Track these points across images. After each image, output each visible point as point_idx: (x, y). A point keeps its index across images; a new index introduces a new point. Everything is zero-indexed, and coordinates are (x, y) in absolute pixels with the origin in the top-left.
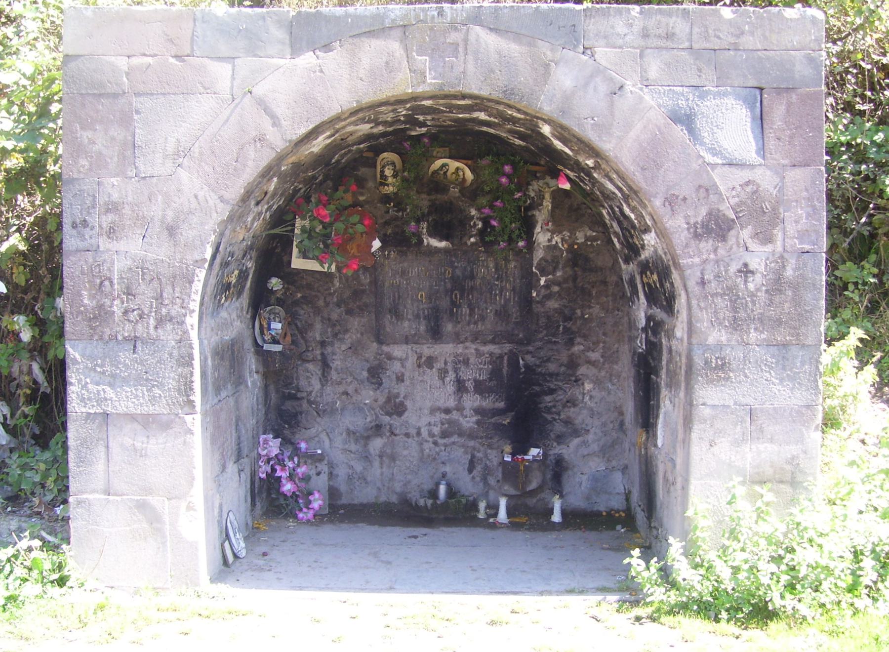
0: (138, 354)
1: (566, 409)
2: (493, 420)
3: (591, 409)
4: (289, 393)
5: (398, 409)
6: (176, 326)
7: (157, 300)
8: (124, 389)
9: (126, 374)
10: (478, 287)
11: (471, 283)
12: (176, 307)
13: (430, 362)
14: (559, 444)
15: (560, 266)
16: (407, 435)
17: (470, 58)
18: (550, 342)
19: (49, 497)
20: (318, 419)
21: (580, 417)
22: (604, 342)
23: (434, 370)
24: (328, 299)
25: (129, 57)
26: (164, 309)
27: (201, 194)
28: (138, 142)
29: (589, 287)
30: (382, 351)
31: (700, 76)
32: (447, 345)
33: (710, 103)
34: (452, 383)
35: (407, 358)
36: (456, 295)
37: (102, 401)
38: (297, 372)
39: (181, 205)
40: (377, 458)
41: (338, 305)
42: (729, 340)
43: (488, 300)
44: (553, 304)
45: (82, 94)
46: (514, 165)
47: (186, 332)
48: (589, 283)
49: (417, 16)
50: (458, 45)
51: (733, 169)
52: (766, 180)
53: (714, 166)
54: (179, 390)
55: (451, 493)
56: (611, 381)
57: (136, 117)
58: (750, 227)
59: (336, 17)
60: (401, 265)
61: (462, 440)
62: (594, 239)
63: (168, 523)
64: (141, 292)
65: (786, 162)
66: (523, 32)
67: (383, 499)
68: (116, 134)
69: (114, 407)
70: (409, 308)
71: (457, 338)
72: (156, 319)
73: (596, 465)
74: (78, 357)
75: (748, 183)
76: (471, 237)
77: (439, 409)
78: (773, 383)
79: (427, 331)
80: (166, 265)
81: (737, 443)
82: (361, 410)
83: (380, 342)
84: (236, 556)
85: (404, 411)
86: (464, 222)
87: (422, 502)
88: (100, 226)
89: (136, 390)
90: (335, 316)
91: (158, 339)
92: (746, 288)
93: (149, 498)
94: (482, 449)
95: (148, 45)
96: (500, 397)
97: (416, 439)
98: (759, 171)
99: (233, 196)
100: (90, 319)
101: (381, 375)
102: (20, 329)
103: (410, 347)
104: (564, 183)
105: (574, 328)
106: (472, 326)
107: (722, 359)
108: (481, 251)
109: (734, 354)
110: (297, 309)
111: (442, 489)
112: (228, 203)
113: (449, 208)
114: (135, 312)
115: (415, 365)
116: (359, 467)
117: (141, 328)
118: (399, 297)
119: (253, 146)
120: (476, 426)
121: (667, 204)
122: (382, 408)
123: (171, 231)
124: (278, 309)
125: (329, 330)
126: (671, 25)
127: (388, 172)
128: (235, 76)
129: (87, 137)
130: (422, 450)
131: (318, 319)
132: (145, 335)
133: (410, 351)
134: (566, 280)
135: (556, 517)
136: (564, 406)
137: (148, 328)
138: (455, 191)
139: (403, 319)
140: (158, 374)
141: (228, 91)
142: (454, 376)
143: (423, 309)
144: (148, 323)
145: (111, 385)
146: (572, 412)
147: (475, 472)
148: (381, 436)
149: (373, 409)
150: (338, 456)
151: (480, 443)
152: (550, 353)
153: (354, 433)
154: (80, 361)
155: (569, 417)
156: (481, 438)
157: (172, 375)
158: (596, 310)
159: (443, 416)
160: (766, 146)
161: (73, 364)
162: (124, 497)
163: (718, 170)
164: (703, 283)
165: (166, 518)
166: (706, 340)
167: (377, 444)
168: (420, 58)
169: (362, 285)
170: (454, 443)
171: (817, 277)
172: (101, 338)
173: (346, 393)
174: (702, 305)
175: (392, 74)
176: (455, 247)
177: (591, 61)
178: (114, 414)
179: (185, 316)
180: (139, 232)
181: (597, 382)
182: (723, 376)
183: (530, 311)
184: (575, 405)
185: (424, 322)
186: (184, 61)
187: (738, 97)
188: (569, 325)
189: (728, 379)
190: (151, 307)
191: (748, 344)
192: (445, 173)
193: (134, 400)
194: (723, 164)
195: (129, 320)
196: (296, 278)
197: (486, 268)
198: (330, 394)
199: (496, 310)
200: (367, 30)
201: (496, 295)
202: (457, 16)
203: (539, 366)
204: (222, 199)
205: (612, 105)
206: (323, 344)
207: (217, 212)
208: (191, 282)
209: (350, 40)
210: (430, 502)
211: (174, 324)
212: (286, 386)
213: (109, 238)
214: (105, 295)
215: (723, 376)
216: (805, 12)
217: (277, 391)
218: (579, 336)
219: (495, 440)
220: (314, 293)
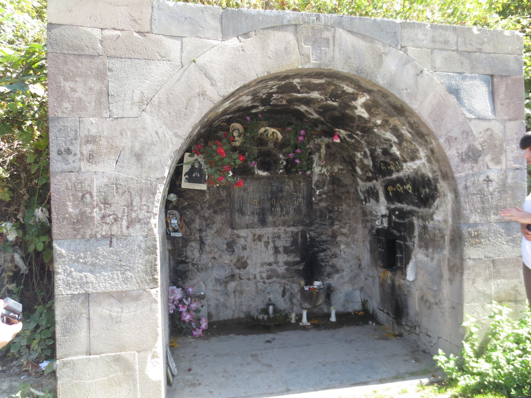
0: (114, 248)
1: (332, 260)
2: (294, 268)
3: (344, 259)
5: (242, 264)
6: (143, 226)
7: (128, 207)
8: (102, 275)
9: (104, 263)
11: (281, 195)
12: (143, 212)
13: (260, 238)
14: (329, 278)
15: (326, 184)
16: (249, 279)
17: (337, 49)
18: (322, 224)
19: (34, 356)
20: (198, 274)
21: (338, 262)
22: (349, 223)
24: (203, 206)
25: (102, 29)
26: (133, 214)
27: (160, 131)
28: (111, 92)
29: (341, 195)
31: (462, 67)
33: (468, 83)
35: (248, 237)
37: (84, 285)
39: (146, 139)
40: (232, 293)
41: (209, 209)
42: (481, 220)
44: (323, 204)
45: (64, 54)
46: (306, 130)
47: (151, 230)
48: (341, 193)
49: (303, 19)
50: (329, 40)
51: (480, 121)
52: (497, 127)
53: (470, 119)
54: (146, 271)
55: (275, 311)
56: (354, 243)
57: (109, 74)
58: (489, 155)
59: (252, 15)
61: (278, 280)
62: (342, 170)
63: (138, 370)
64: (115, 201)
65: (506, 118)
66: (367, 34)
67: (236, 316)
68: (93, 85)
69: (94, 288)
70: (248, 209)
71: (275, 224)
72: (128, 221)
73: (347, 288)
74: (64, 252)
75: (488, 130)
76: (280, 169)
77: (265, 263)
78: (503, 244)
79: (259, 221)
80: (135, 182)
81: (487, 280)
82: (223, 267)
83: (233, 228)
84: (173, 375)
85: (247, 266)
86: (277, 161)
87: (261, 317)
88: (82, 153)
89: (112, 274)
90: (207, 215)
91: (129, 235)
92: (488, 190)
93: (123, 353)
94: (289, 284)
95: (117, 22)
97: (254, 281)
98: (493, 123)
99: (184, 133)
100: (74, 223)
101: (234, 247)
102: (7, 232)
104: (336, 139)
105: (334, 217)
107: (477, 231)
108: (286, 177)
109: (484, 229)
110: (185, 211)
111: (271, 308)
112: (181, 137)
113: (268, 154)
114: (111, 217)
116: (222, 300)
117: (115, 228)
118: (243, 203)
119: (197, 99)
121: (447, 141)
122: (235, 265)
123: (139, 157)
124: (175, 212)
125: (204, 223)
126: (447, 36)
127: (235, 134)
128: (183, 50)
129: (69, 86)
130: (257, 287)
131: (198, 217)
132: (119, 233)
133: (249, 233)
134: (329, 192)
135: (333, 319)
136: (331, 258)
137: (121, 228)
138: (271, 145)
139: (245, 215)
140: (129, 261)
141: (179, 60)
142: (273, 245)
143: (256, 209)
144: (121, 224)
145: (91, 272)
146: (334, 261)
147: (286, 297)
149: (230, 266)
150: (210, 294)
151: (288, 281)
152: (322, 230)
153: (219, 280)
154: (65, 255)
155: (334, 264)
156: (289, 278)
157: (140, 261)
158: (344, 207)
159: (268, 267)
160: (496, 109)
161: (59, 258)
162: (102, 355)
163: (473, 122)
164: (466, 188)
165: (137, 367)
166: (469, 221)
167: (232, 285)
168: (306, 46)
169: (222, 197)
170: (274, 282)
171: (523, 183)
172: (83, 237)
173: (214, 258)
174: (466, 200)
175: (289, 55)
177: (405, 55)
178: (94, 293)
179: (150, 218)
180: (112, 158)
181: (347, 245)
182: (478, 241)
183: (312, 208)
184: (336, 257)
185: (256, 216)
186: (145, 36)
187: (482, 79)
188: (331, 215)
189: (480, 243)
190: (124, 212)
191: (490, 222)
192: (267, 135)
193: (110, 282)
194: (475, 119)
195: (106, 223)
196: (184, 194)
197: (289, 187)
198: (205, 259)
199: (295, 209)
200: (273, 25)
201: (294, 200)
202: (328, 21)
203: (317, 237)
204: (176, 134)
205: (416, 82)
206: (200, 231)
207: (173, 144)
208: (154, 194)
209: (262, 31)
210: (266, 317)
211: (141, 225)
212: (179, 256)
213: (90, 162)
214: (87, 204)
215: (478, 241)
216: (514, 32)
218: (337, 221)
219: (295, 278)
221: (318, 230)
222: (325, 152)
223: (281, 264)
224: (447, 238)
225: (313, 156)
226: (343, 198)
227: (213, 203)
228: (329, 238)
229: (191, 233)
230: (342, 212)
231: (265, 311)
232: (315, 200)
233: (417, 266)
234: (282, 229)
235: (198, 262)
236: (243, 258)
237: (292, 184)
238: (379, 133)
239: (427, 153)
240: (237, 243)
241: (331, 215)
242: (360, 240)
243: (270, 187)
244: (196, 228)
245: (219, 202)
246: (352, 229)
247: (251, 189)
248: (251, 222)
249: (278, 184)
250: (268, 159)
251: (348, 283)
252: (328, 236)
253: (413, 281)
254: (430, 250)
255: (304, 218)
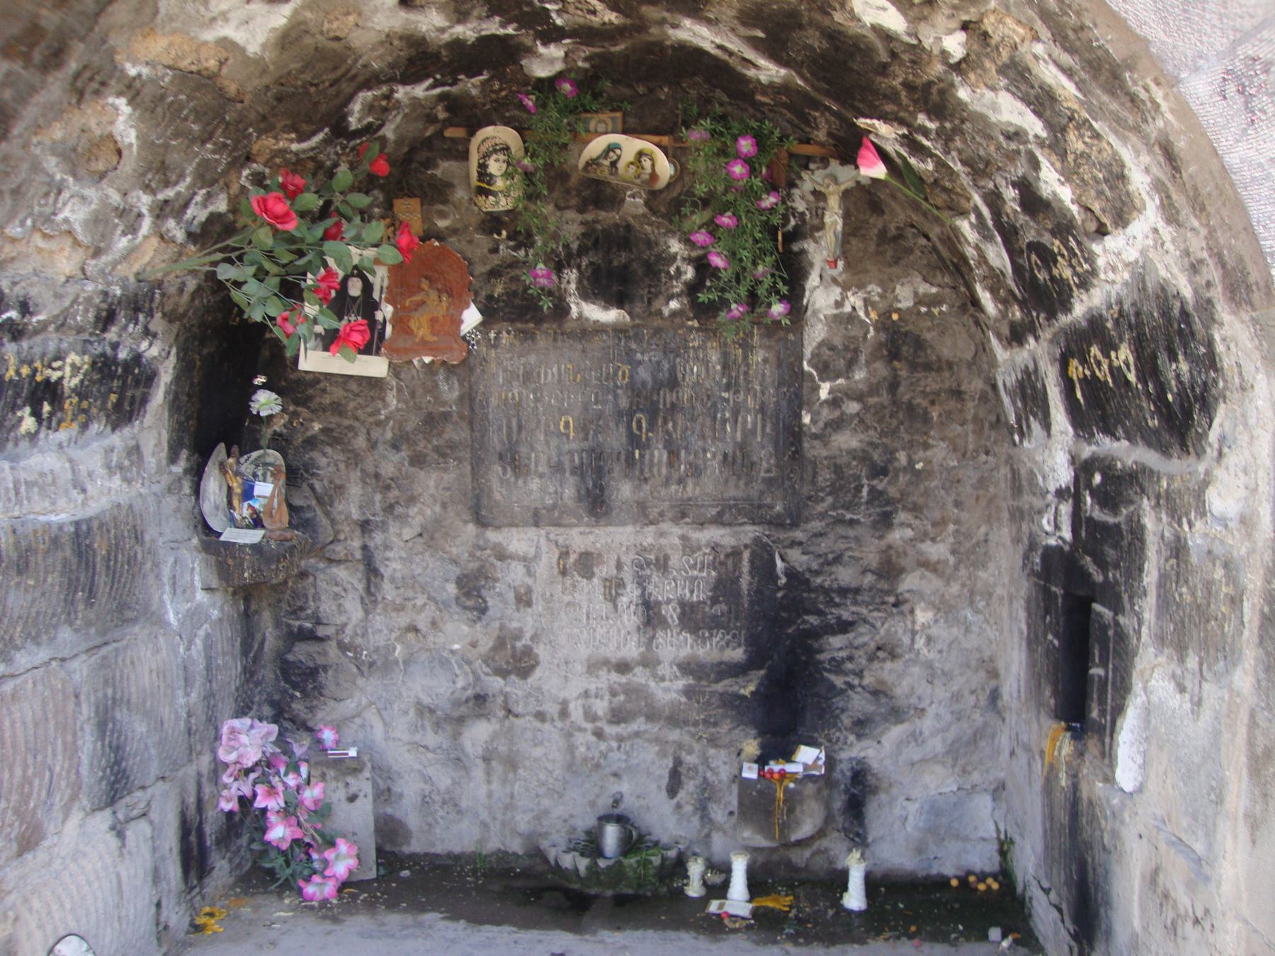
1: (876, 665)
2: (719, 687)
3: (929, 665)
4: (300, 628)
10: (687, 405)
11: (670, 397)
13: (587, 563)
14: (859, 737)
15: (863, 358)
16: (541, 716)
18: (840, 521)
20: (361, 682)
22: (957, 522)
23: (595, 580)
30: (487, 541)
32: (620, 529)
34: (633, 607)
35: (537, 557)
36: (639, 422)
38: (315, 586)
40: (479, 762)
41: (395, 446)
43: (708, 433)
44: (847, 440)
48: (924, 394)
60: (523, 360)
61: (654, 728)
67: (493, 844)
70: (540, 451)
71: (642, 514)
76: (671, 297)
77: (606, 662)
79: (579, 499)
82: (444, 663)
83: (482, 522)
86: (656, 267)
87: (567, 861)
90: (388, 469)
94: (696, 747)
96: (734, 636)
97: (559, 724)
101: (484, 592)
103: (543, 532)
105: (893, 492)
106: (674, 487)
108: (691, 329)
110: (315, 454)
113: (623, 238)
115: (556, 571)
118: (520, 427)
120: (683, 699)
121: (1231, 89)
125: (378, 497)
130: (571, 749)
131: (356, 475)
133: (543, 541)
135: (854, 899)
136: (872, 658)
138: (635, 204)
139: (528, 473)
142: (637, 592)
143: (570, 452)
146: (887, 671)
147: (682, 795)
148: (486, 716)
149: (469, 662)
150: (400, 757)
151: (693, 735)
152: (842, 545)
153: (432, 711)
155: (882, 682)
156: (696, 724)
158: (940, 452)
159: (615, 677)
167: (479, 733)
169: (444, 404)
170: (637, 734)
176: (637, 321)
181: (944, 608)
183: (797, 455)
184: (893, 656)
188: (880, 484)
192: (614, 164)
196: (310, 391)
199: (725, 455)
201: (724, 421)
203: (817, 573)
206: (365, 526)
210: (583, 864)
212: (294, 612)
217: (277, 624)
218: (904, 508)
219: (724, 728)
220: (346, 422)
221: (824, 546)
222: (840, 222)
223: (665, 669)
224: (1251, 610)
225: (809, 245)
226: (935, 415)
227: (410, 426)
228: (869, 579)
229: (337, 533)
230: (927, 473)
231: (592, 845)
232: (813, 421)
233: (1148, 733)
234: (674, 533)
235: (359, 640)
236: (518, 636)
237: (714, 357)
238: (977, 108)
239: (1155, 170)
240: (496, 580)
241: (880, 484)
242: (999, 591)
243: (626, 368)
244: (348, 516)
245: (433, 422)
246: (968, 545)
247: (550, 374)
248: (549, 502)
249: (656, 356)
250: (621, 258)
251: (944, 764)
252: (865, 571)
253: (1131, 794)
254: (1192, 662)
255: (762, 493)
